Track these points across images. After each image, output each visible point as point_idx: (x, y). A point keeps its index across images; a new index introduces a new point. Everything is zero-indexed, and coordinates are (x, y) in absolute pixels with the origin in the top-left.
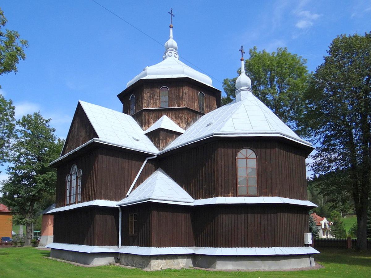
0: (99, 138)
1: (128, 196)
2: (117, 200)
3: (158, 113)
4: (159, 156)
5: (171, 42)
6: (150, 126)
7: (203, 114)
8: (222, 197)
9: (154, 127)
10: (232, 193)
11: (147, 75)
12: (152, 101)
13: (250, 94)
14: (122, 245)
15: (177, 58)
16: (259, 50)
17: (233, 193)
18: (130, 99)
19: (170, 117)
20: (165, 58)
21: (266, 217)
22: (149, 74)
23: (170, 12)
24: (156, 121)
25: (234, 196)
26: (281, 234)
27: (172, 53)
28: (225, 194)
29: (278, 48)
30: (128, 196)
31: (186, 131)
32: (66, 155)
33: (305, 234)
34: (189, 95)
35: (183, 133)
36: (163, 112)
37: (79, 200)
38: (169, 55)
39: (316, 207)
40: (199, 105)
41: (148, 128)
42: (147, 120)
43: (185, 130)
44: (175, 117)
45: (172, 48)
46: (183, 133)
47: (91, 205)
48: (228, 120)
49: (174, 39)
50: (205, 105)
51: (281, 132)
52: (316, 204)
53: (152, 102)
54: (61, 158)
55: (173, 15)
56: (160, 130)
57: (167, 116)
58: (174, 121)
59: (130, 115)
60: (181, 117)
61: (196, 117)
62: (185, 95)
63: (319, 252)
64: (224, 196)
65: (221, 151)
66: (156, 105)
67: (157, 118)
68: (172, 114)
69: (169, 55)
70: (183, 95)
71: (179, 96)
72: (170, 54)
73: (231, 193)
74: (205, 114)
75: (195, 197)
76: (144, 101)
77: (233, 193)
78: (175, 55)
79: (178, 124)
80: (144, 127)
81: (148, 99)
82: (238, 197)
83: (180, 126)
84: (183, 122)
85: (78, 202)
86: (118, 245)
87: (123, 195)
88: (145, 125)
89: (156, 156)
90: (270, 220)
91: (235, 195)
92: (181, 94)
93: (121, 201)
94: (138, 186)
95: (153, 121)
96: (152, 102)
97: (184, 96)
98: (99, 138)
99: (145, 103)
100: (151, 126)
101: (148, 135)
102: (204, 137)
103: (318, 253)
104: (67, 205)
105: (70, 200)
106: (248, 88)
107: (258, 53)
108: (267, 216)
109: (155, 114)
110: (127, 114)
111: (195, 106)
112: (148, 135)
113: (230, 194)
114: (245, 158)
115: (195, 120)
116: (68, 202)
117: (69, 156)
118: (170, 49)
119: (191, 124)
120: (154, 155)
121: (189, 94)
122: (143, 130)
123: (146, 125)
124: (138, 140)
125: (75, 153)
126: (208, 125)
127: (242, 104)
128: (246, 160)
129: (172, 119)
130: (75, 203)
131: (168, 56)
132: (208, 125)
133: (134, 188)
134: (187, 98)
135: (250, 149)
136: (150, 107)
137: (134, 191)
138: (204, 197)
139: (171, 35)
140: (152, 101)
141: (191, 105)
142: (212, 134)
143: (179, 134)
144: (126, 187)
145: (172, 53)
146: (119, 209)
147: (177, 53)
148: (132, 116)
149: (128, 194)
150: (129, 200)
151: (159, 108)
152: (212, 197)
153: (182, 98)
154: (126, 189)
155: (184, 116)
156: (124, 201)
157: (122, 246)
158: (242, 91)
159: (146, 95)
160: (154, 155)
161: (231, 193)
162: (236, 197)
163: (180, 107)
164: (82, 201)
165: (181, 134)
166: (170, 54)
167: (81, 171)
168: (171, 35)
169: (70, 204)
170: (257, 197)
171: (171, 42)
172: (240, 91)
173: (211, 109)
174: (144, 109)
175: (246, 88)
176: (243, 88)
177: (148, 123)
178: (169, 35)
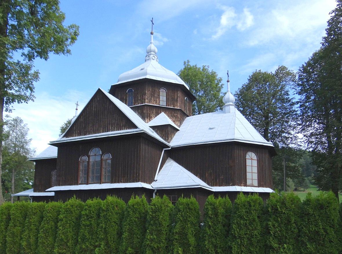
3: (158, 110)
11: (147, 75)
12: (153, 98)
13: (233, 107)
15: (158, 62)
16: (192, 64)
18: (127, 92)
20: (148, 60)
22: (149, 74)
24: (156, 116)
25: (244, 186)
29: (203, 66)
41: (150, 121)
45: (154, 52)
53: (153, 100)
57: (165, 113)
58: (170, 118)
65: (237, 152)
66: (156, 102)
67: (157, 114)
71: (174, 98)
72: (154, 58)
76: (146, 97)
79: (174, 121)
80: (146, 120)
89: (170, 148)
90: (41, 203)
91: (246, 185)
96: (153, 100)
99: (147, 98)
107: (202, 68)
113: (242, 184)
114: (250, 159)
120: (169, 147)
122: (146, 123)
128: (251, 160)
131: (152, 59)
135: (254, 153)
136: (151, 103)
138: (90, 179)
140: (153, 98)
151: (158, 106)
159: (148, 93)
160: (169, 147)
162: (246, 187)
163: (175, 108)
166: (154, 58)
170: (258, 188)
174: (146, 104)
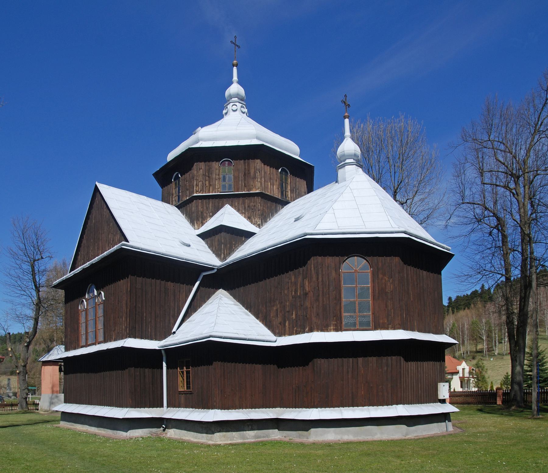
0: (128, 242)
1: (174, 333)
2: (160, 339)
4: (221, 270)
5: (235, 88)
6: (205, 222)
7: (287, 203)
8: (318, 332)
9: (211, 224)
10: (333, 326)
14: (168, 406)
17: (336, 325)
19: (235, 208)
21: (384, 361)
23: (234, 42)
26: (406, 388)
27: (236, 106)
28: (324, 328)
30: (174, 333)
31: (261, 229)
32: (79, 270)
33: (440, 384)
34: (265, 173)
35: (256, 233)
36: (225, 200)
37: (101, 338)
38: (232, 110)
39: (455, 344)
40: (280, 189)
42: (200, 213)
43: (259, 228)
44: (243, 208)
46: (256, 233)
47: (120, 346)
48: (327, 212)
49: (239, 83)
50: (289, 188)
51: (407, 230)
52: (454, 338)
54: (69, 275)
55: (237, 46)
56: (221, 229)
57: (232, 206)
59: (174, 205)
60: (253, 207)
61: (276, 207)
62: (258, 172)
63: (459, 410)
64: (322, 330)
68: (239, 203)
69: (232, 110)
70: (255, 173)
73: (332, 325)
74: (289, 203)
75: (279, 332)
77: (335, 326)
78: (242, 109)
81: (202, 180)
82: (343, 332)
83: (252, 222)
84: (256, 214)
85: (100, 343)
86: (162, 406)
87: (167, 332)
88: (198, 220)
91: (338, 328)
92: (252, 171)
93: (164, 341)
94: (195, 310)
95: (209, 214)
97: (258, 174)
98: (128, 242)
100: (206, 222)
101: (203, 236)
102: (303, 235)
103: (458, 412)
104: (82, 347)
105: (87, 339)
106: (355, 161)
108: (387, 360)
109: (212, 203)
110: (169, 204)
111: (276, 193)
112: (203, 236)
113: (332, 328)
115: (272, 212)
116: (83, 343)
117: (84, 270)
118: (233, 99)
119: (268, 220)
121: (264, 171)
123: (199, 220)
124: (189, 246)
125: (92, 265)
126: (297, 220)
127: (348, 187)
129: (238, 211)
130: (94, 344)
132: (297, 220)
133: (187, 315)
134: (262, 178)
137: (184, 325)
139: (235, 78)
141: (267, 188)
142: (305, 234)
143: (249, 235)
144: (171, 318)
145: (236, 106)
146: (163, 352)
147: (244, 106)
148: (176, 207)
149: (174, 330)
150: (176, 338)
152: (305, 333)
153: (255, 178)
154: (172, 321)
155: (257, 206)
156: (171, 341)
157: (169, 408)
158: (346, 167)
160: (213, 269)
161: (332, 325)
164: (105, 341)
165: (254, 234)
167: (103, 293)
168: (235, 78)
169: (87, 345)
171: (235, 88)
172: (343, 166)
173: (298, 195)
174: (195, 195)
175: (352, 161)
176: (348, 161)
177: (202, 218)
178: (232, 77)
